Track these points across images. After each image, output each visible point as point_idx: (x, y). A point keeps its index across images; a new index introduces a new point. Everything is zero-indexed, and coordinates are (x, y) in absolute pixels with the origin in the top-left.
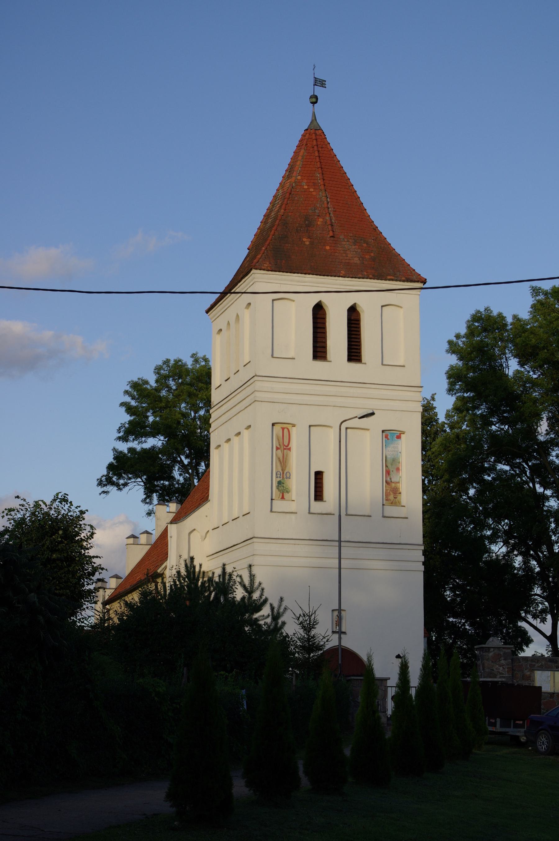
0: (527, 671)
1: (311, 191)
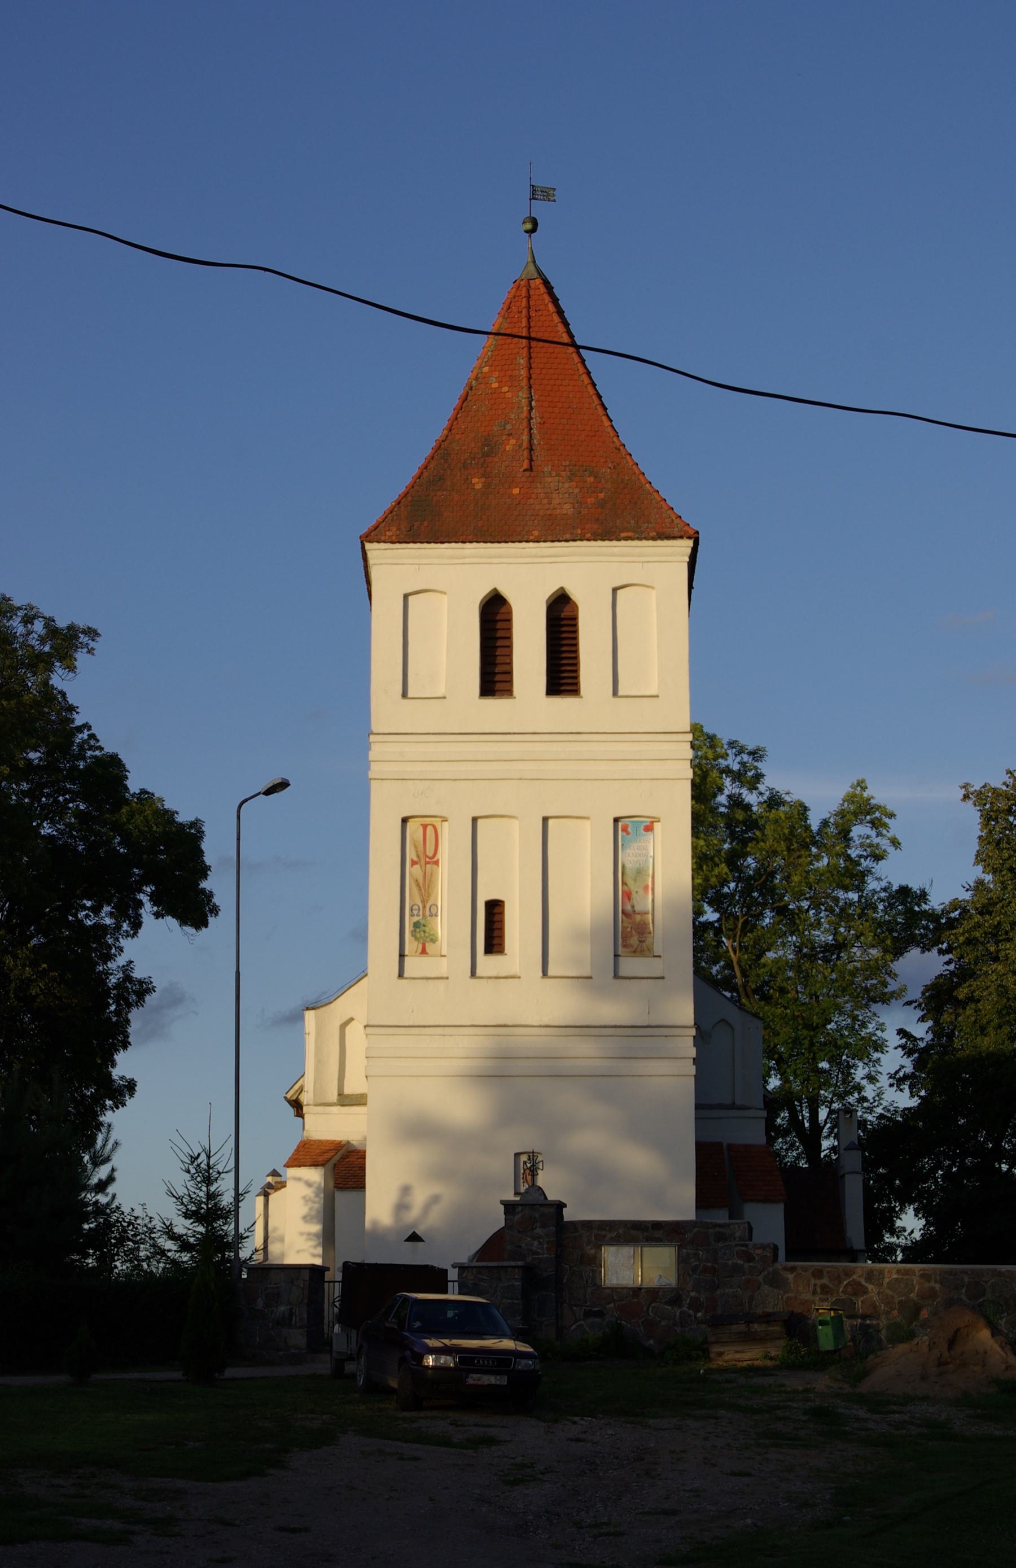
0: (590, 1247)
1: (503, 391)
